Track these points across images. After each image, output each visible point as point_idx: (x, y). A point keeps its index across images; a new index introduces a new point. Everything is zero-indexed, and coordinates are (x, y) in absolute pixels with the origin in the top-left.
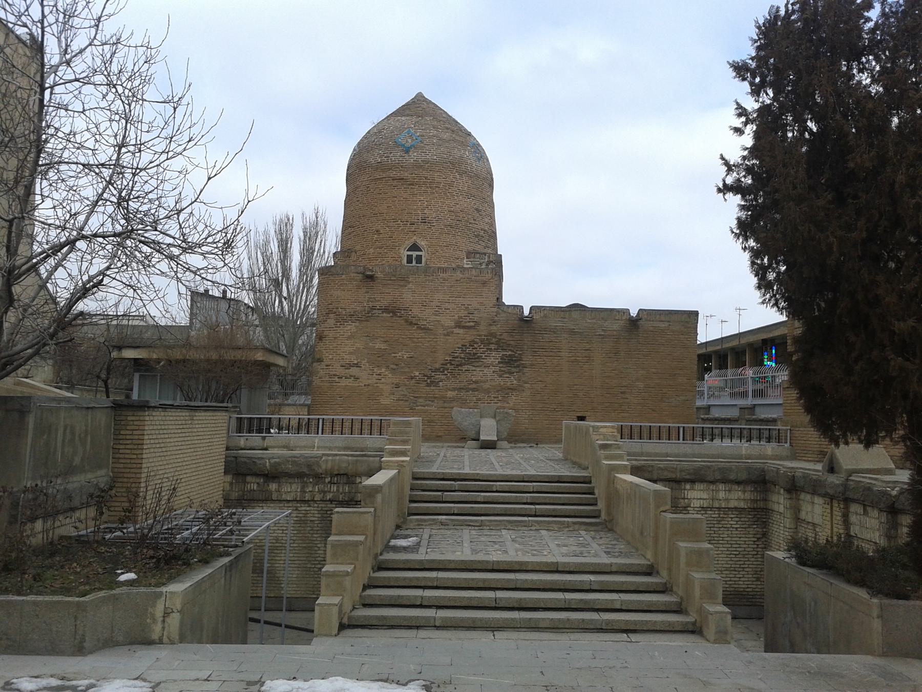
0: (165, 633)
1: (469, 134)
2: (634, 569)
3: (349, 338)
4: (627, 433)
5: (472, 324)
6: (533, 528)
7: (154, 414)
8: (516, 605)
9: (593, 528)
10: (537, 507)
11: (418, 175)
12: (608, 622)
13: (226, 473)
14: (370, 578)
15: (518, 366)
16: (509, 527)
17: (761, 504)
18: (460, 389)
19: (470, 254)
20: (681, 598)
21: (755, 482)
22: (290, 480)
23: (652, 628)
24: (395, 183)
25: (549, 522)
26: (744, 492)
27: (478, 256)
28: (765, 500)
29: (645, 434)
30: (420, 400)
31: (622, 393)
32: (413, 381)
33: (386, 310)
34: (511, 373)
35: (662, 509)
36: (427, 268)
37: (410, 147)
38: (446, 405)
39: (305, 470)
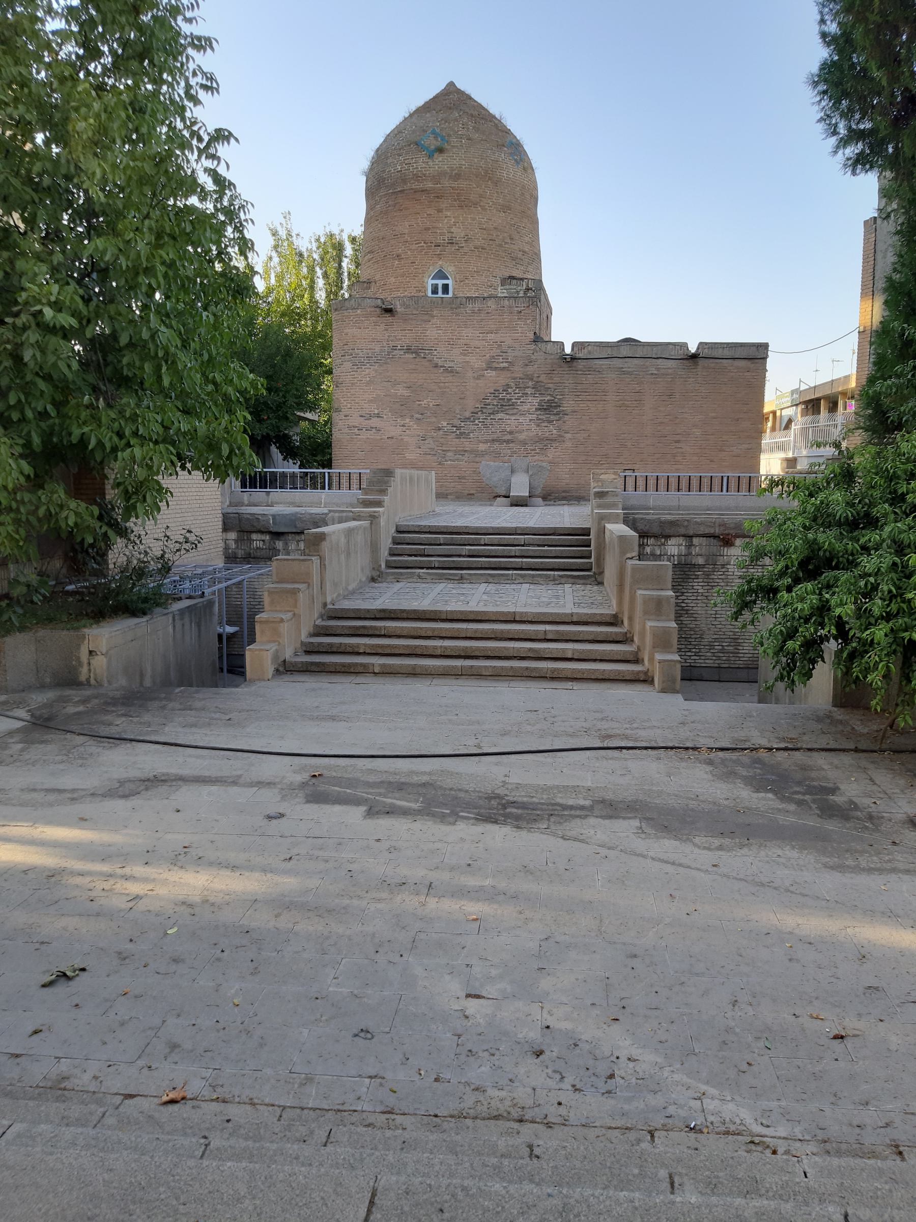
0: (92, 675)
2: (598, 619)
3: (368, 383)
5: (506, 365)
6: (517, 581)
9: (582, 581)
10: (525, 560)
12: (554, 670)
13: (225, 529)
14: (316, 626)
16: (491, 580)
23: (601, 677)
25: (533, 576)
30: (449, 454)
32: (441, 432)
33: (409, 350)
34: (550, 422)
35: (629, 555)
36: (455, 297)
38: (477, 459)
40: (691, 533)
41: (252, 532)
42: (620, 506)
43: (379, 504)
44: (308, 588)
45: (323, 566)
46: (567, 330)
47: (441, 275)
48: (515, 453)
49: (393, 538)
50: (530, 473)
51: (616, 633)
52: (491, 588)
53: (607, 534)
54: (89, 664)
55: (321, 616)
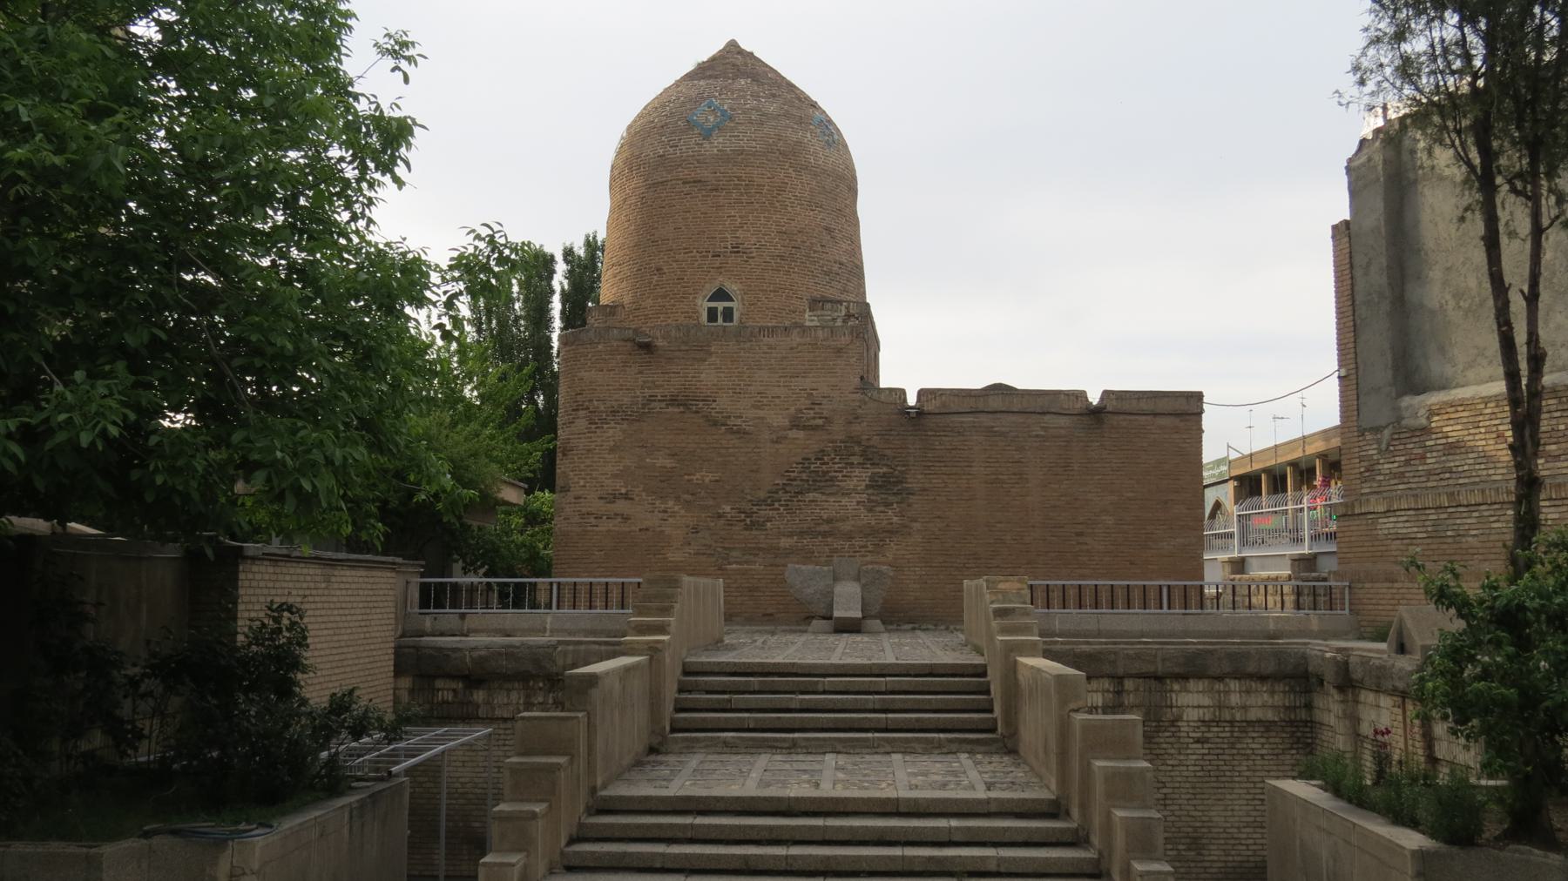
1: (814, 105)
3: (612, 450)
4: (1046, 597)
5: (820, 422)
7: (255, 568)
9: (982, 749)
11: (739, 173)
13: (398, 672)
14: (581, 825)
16: (840, 748)
17: (1303, 715)
18: (802, 534)
19: (816, 303)
20: (1100, 853)
21: (1292, 677)
22: (509, 685)
24: (687, 188)
25: (907, 740)
26: (1272, 693)
27: (828, 306)
28: (1309, 706)
29: (1088, 600)
30: (734, 554)
31: (1078, 534)
34: (888, 505)
35: (1072, 706)
36: (742, 326)
37: (712, 130)
40: (1120, 671)
41: (435, 677)
42: (1036, 630)
43: (661, 629)
44: (571, 762)
45: (591, 726)
47: (721, 295)
48: (835, 551)
49: (680, 682)
51: (1062, 831)
52: (842, 760)
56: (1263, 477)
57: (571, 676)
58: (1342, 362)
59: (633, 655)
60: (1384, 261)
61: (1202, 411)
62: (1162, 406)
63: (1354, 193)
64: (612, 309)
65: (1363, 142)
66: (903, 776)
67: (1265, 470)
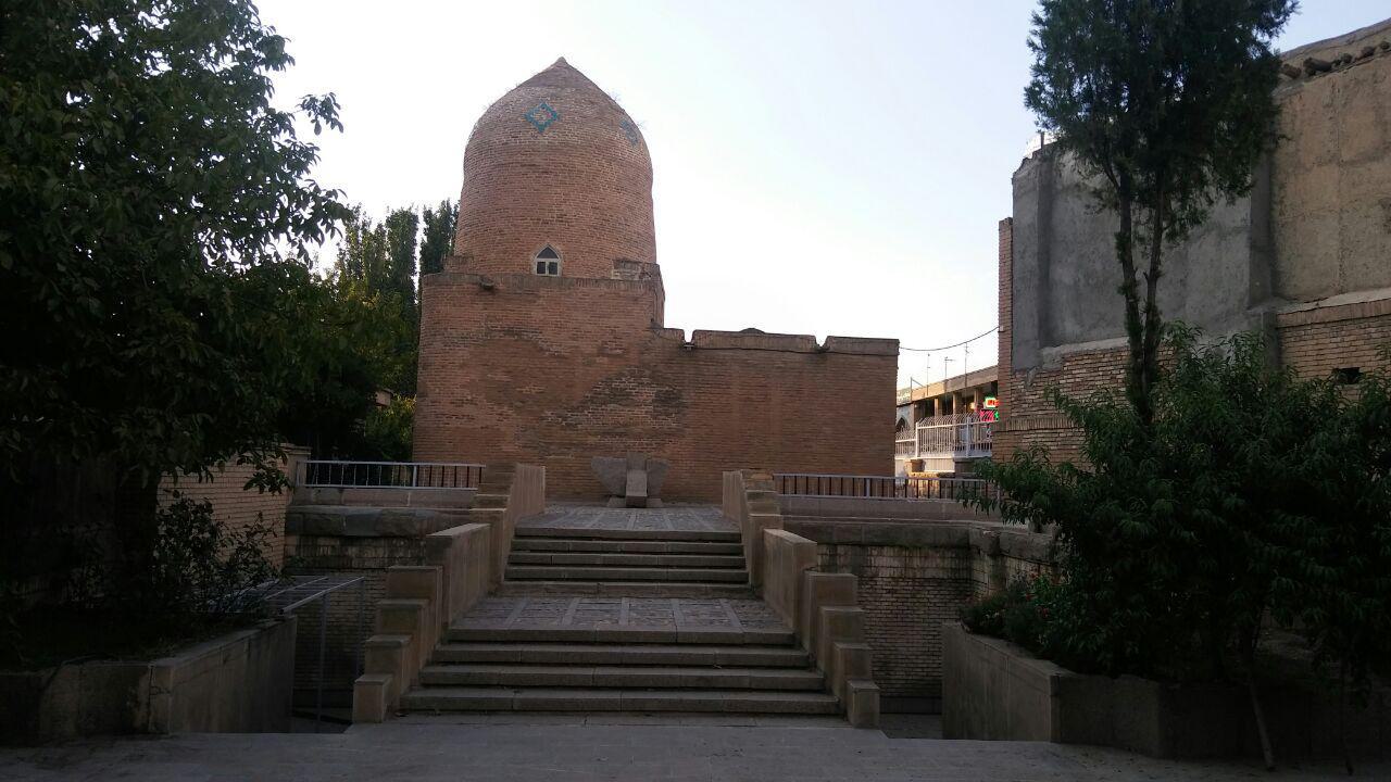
0: (151, 718)
3: (462, 366)
6: (663, 595)
8: (619, 684)
9: (738, 596)
11: (560, 155)
12: (730, 703)
14: (435, 652)
15: (677, 406)
16: (632, 594)
17: (964, 575)
19: (620, 263)
20: (825, 674)
24: (524, 170)
26: (943, 558)
27: (629, 265)
28: (970, 570)
30: (552, 447)
34: (668, 415)
36: (564, 277)
38: (587, 453)
39: (394, 531)
40: (835, 540)
41: (318, 536)
43: (500, 503)
44: (429, 604)
45: (445, 577)
46: (685, 312)
48: (629, 447)
50: (648, 470)
52: (634, 603)
53: (766, 537)
54: (148, 704)
55: (442, 642)
56: (936, 401)
57: (431, 538)
58: (1001, 321)
59: (478, 522)
60: (1035, 248)
61: (898, 354)
62: (868, 349)
63: (1016, 198)
64: (464, 259)
65: (1025, 160)
66: (680, 615)
67: (936, 397)
